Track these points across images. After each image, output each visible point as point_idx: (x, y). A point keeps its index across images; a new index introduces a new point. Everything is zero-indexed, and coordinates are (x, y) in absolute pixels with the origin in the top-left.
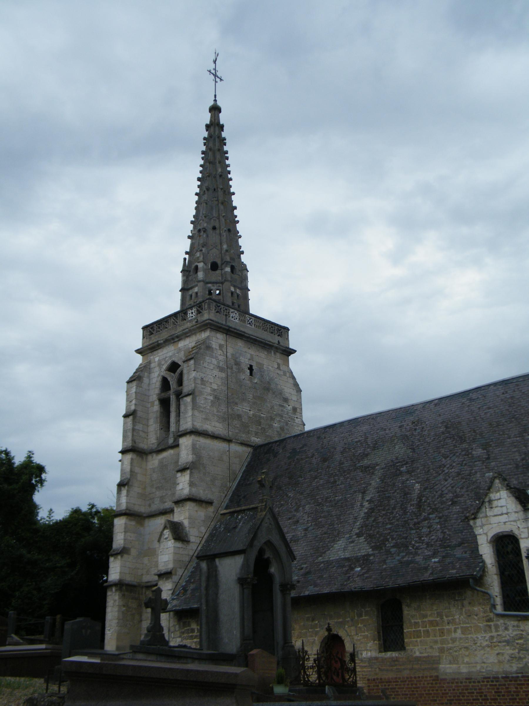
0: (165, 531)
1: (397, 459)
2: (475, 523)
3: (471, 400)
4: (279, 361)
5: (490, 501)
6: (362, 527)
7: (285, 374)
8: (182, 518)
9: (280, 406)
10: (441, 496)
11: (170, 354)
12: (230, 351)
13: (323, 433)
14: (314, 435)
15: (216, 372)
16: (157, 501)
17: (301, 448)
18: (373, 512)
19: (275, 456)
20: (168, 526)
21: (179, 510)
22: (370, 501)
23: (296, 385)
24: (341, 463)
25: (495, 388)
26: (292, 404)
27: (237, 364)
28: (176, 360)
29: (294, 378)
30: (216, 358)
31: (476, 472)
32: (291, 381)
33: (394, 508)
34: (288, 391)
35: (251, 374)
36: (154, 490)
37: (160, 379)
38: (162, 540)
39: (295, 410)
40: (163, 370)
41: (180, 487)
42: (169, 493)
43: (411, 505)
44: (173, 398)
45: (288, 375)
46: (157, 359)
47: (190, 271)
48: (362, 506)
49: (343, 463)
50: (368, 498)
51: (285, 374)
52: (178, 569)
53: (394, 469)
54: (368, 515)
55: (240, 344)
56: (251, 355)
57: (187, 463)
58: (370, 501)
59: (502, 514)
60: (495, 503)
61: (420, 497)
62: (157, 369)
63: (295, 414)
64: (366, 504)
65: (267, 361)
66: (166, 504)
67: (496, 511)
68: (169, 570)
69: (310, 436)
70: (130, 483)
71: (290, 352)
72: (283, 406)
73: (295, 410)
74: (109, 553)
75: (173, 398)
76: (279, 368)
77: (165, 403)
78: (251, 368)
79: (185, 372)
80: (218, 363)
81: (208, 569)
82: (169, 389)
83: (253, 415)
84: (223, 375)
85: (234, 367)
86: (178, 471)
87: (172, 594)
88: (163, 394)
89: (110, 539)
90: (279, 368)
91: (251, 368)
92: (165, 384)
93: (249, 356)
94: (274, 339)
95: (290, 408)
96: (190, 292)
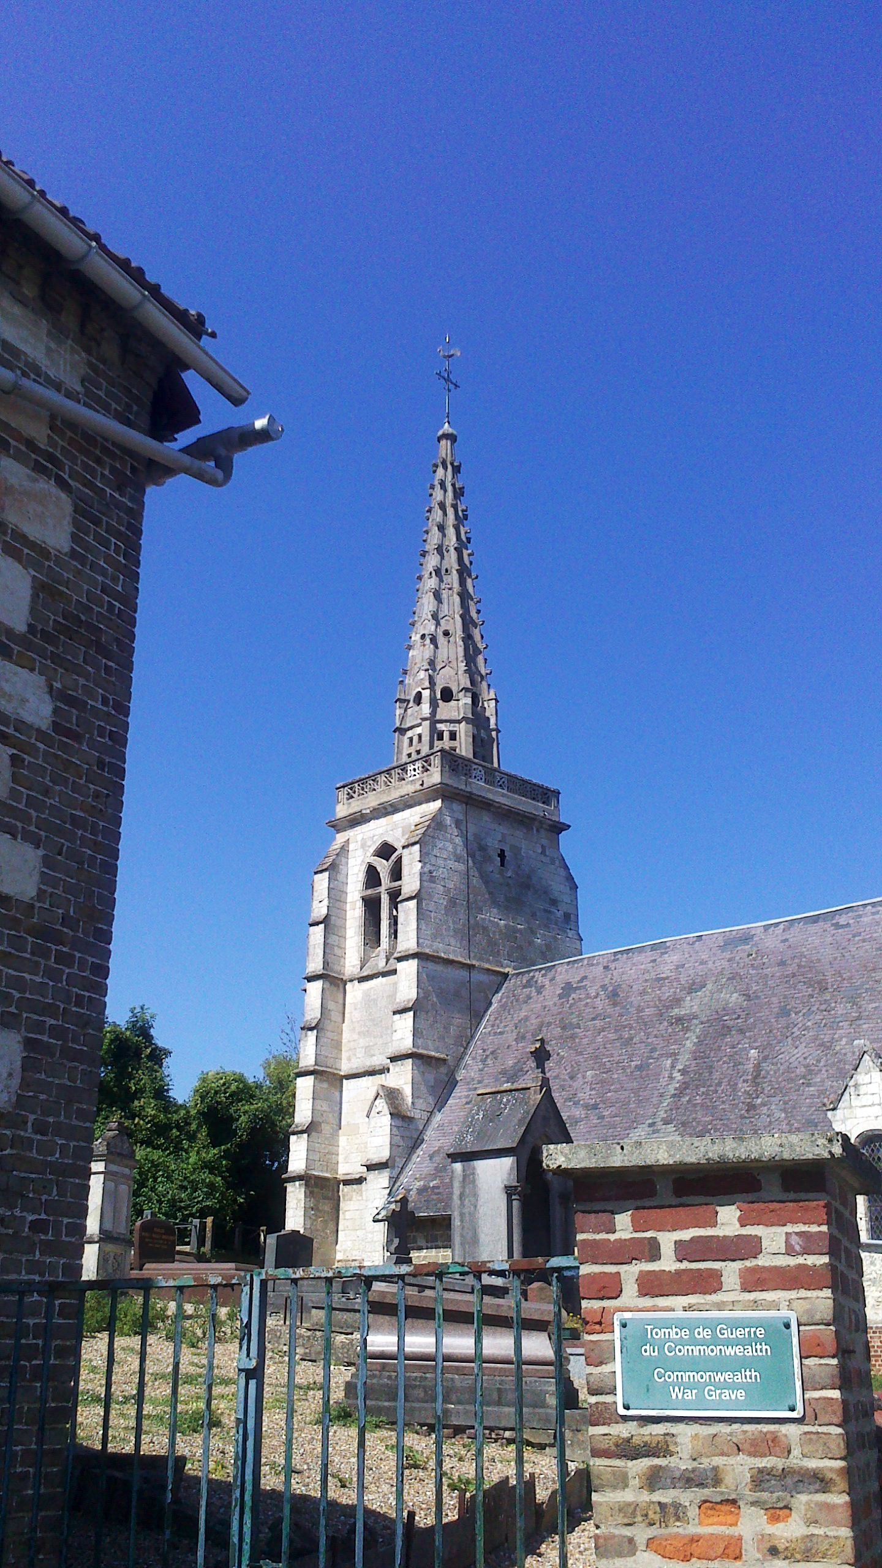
0: (378, 1101)
1: (724, 1009)
2: (835, 1116)
3: (837, 926)
4: (544, 842)
5: (856, 1086)
6: (671, 1110)
7: (553, 862)
8: (402, 1082)
9: (545, 911)
10: (789, 1070)
11: (381, 831)
12: (472, 829)
13: (614, 961)
14: (598, 964)
15: (451, 864)
16: (360, 1053)
17: (579, 982)
18: (685, 1089)
19: (539, 992)
20: (381, 1093)
21: (397, 1069)
22: (683, 1072)
23: (570, 878)
24: (640, 1010)
25: (874, 910)
26: (563, 908)
27: (483, 848)
28: (390, 841)
29: (566, 868)
30: (451, 841)
31: (841, 1039)
32: (562, 872)
33: (719, 1084)
34: (558, 888)
35: (502, 865)
36: (356, 1036)
37: (364, 868)
38: (373, 1113)
39: (567, 917)
40: (369, 854)
41: (396, 1036)
42: (380, 1041)
43: (744, 1081)
44: (385, 900)
45: (557, 862)
46: (359, 838)
47: (409, 701)
48: (671, 1078)
49: (643, 1010)
50: (681, 1067)
51: (553, 862)
52: (398, 1159)
53: (721, 1026)
54: (678, 1095)
55: (486, 818)
56: (503, 835)
57: (409, 1001)
58: (683, 1072)
59: (873, 1105)
60: (863, 1090)
61: (758, 1067)
62: (360, 852)
63: (567, 923)
64: (678, 1076)
65: (527, 846)
66: (375, 1058)
67: (865, 1100)
68: (384, 1160)
69: (593, 965)
70: (321, 1026)
71: (559, 828)
72: (550, 912)
73: (567, 917)
74: (290, 1130)
75: (385, 900)
76: (543, 853)
77: (372, 906)
78: (502, 854)
79: (405, 861)
80: (455, 848)
81: (464, 1171)
82: (379, 884)
83: (506, 925)
84: (462, 867)
85: (478, 853)
86: (395, 1013)
87: (389, 1194)
88: (369, 892)
89: (289, 1110)
90: (543, 853)
91: (502, 854)
92: (372, 877)
93: (499, 837)
94: (536, 808)
95: (559, 914)
96: (409, 734)
